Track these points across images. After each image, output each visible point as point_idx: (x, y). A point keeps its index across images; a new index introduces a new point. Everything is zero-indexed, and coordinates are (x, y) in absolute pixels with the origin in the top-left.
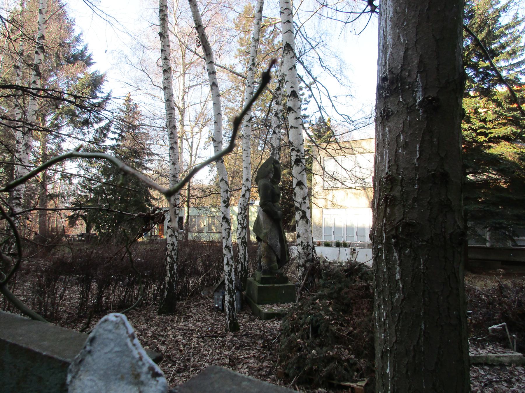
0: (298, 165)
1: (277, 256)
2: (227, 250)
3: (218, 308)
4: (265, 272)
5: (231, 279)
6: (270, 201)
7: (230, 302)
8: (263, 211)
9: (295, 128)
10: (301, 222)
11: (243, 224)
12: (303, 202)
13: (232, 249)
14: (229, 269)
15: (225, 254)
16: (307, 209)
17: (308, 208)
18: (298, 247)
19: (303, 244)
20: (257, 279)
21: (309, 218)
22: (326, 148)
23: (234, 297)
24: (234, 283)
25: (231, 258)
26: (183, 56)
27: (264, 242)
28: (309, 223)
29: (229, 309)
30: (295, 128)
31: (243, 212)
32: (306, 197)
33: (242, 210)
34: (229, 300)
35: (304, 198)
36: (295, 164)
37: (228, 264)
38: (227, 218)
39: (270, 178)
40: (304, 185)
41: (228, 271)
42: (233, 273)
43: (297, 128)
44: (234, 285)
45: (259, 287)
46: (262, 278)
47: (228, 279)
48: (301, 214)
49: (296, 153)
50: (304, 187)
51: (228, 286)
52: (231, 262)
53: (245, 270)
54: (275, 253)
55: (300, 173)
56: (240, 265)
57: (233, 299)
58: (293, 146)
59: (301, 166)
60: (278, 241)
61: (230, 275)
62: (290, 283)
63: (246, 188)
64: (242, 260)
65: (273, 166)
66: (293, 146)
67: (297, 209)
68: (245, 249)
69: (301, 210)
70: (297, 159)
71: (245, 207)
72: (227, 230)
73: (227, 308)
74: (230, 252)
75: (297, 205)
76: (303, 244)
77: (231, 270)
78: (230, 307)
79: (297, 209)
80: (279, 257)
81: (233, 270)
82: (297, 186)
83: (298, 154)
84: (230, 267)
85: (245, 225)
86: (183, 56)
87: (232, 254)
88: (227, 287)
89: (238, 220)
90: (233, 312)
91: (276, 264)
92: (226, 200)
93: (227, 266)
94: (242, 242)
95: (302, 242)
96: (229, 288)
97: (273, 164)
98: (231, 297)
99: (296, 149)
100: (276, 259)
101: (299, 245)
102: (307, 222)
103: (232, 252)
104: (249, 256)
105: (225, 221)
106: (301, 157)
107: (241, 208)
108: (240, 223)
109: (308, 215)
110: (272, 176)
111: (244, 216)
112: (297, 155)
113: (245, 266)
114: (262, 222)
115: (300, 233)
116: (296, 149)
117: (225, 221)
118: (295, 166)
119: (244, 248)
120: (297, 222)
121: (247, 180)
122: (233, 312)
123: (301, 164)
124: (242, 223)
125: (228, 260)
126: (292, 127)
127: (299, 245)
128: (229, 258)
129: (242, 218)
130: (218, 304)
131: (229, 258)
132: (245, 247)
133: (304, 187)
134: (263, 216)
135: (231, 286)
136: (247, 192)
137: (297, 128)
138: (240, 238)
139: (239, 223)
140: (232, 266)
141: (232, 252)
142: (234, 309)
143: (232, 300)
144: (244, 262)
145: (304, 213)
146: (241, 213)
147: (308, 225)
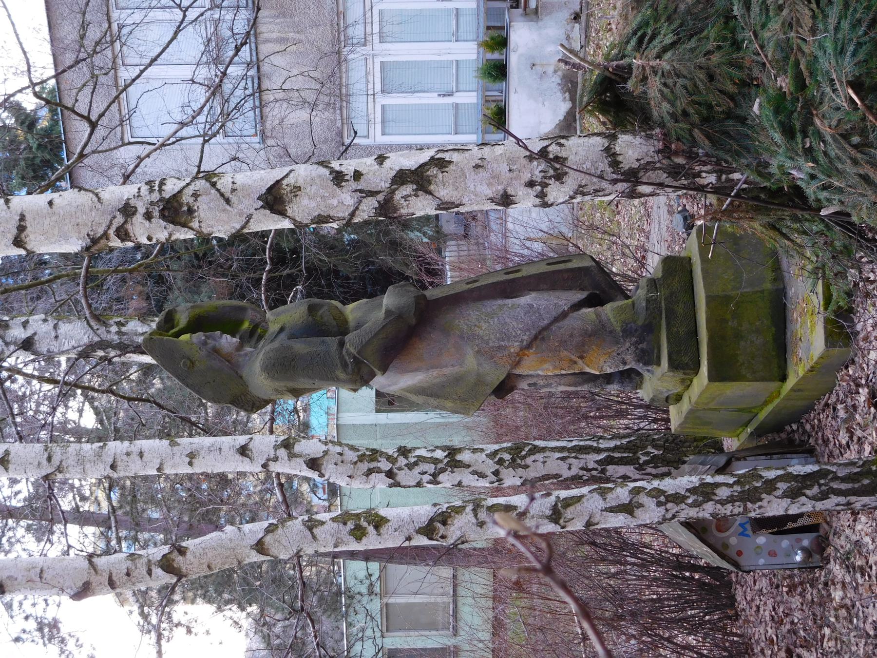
0: (191, 211)
1: (577, 306)
2: (569, 513)
3: (807, 552)
4: (649, 358)
5: (693, 491)
6: (342, 344)
7: (793, 495)
8: (384, 370)
9: (21, 228)
10: (445, 193)
11: (436, 461)
12: (354, 185)
13: (564, 494)
14: (649, 502)
15: (589, 524)
16: (387, 163)
17: (381, 159)
18: (550, 199)
19: (538, 177)
20: (679, 389)
21: (425, 157)
22: (87, 118)
23: (771, 474)
24: (709, 479)
25: (603, 493)
26: (84, 60)
27: (518, 364)
28: (447, 156)
29: (823, 496)
30: (21, 228)
31: (385, 465)
32: (332, 171)
33: (379, 471)
34: (785, 495)
35: (338, 178)
36: (184, 225)
37: (628, 509)
38: (432, 520)
39: (240, 347)
40: (278, 182)
41: (659, 504)
42: (669, 485)
43: (22, 218)
44: (720, 479)
45: (712, 378)
46: (674, 366)
47: (696, 504)
48: (407, 189)
49: (138, 218)
50: (290, 180)
51: (723, 503)
52: (622, 494)
53: (632, 448)
54: (564, 315)
55: (228, 201)
56: (611, 469)
57: (779, 478)
58: (105, 235)
59: (196, 195)
60: (510, 302)
61: (677, 498)
62: (692, 248)
63: (282, 453)
64: (592, 459)
65: (185, 337)
66: (105, 235)
67: (386, 207)
68: (543, 449)
69: (393, 192)
70: (163, 216)
71: (362, 458)
72: (483, 515)
73: (820, 506)
74: (579, 499)
75: (367, 210)
76: (538, 177)
77: (656, 493)
78: (815, 490)
79: (386, 207)
80: (580, 296)
81: (656, 483)
82: (283, 213)
83: (142, 210)
84: (643, 499)
85: (440, 454)
86: (84, 60)
87: (585, 490)
88: (728, 509)
89: (419, 485)
90: (836, 478)
91: (608, 309)
92: (350, 525)
93: (638, 512)
94: (513, 464)
95: (531, 184)
96: (731, 500)
97: (178, 335)
98: (770, 486)
99: (120, 219)
100: (588, 312)
101: (542, 195)
102: (441, 164)
103: (575, 492)
104: (577, 433)
105: (442, 529)
106: (155, 196)
107: (369, 472)
108: (434, 475)
109: (411, 161)
110: (227, 342)
111: (402, 461)
112: (148, 216)
113: (616, 449)
114: (434, 373)
115: (489, 193)
116: (120, 219)
117: (442, 529)
118: (195, 224)
119: (539, 457)
120: (445, 206)
121: (244, 451)
122: (836, 478)
123: (186, 198)
124: (430, 468)
125: (612, 510)
126: (18, 242)
127: (542, 195)
128: (601, 504)
129: (410, 466)
130: (790, 553)
131: (601, 504)
132: (535, 450)
133: (290, 180)
134: (405, 371)
135: (723, 493)
136: (298, 448)
137: (22, 218)
138: (496, 473)
139: (435, 481)
140: (637, 491)
141: (575, 492)
142: (822, 474)
143: (782, 486)
144: (598, 451)
145: (401, 177)
146: (390, 474)
147: (455, 157)
